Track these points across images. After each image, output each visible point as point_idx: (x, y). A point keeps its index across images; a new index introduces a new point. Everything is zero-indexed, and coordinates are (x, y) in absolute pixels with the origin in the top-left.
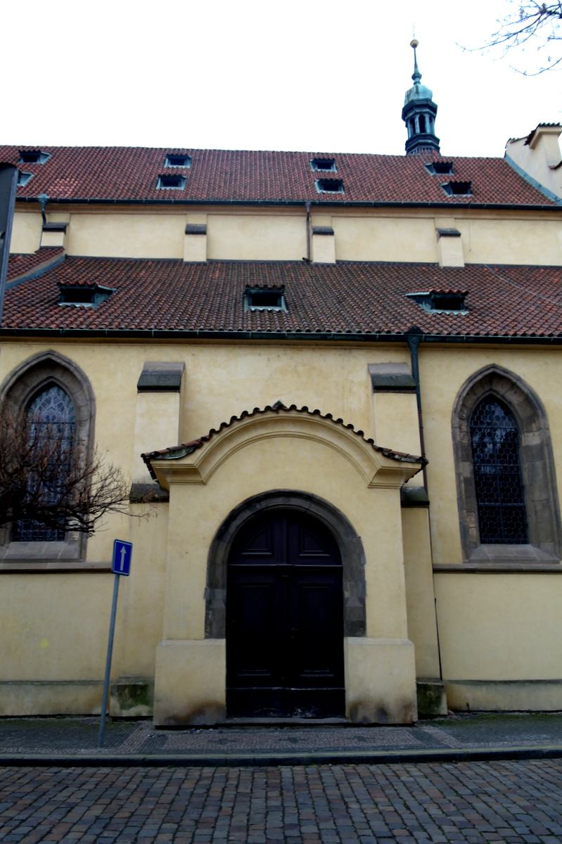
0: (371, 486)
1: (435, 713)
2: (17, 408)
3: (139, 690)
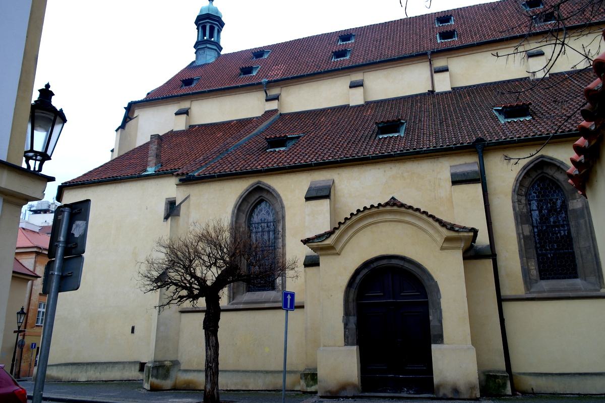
0: (442, 249)
1: (502, 394)
2: (244, 216)
3: (311, 376)
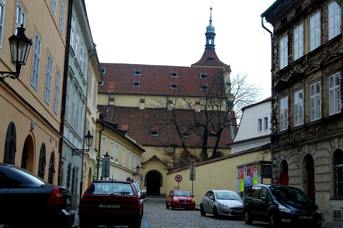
0: (164, 170)
